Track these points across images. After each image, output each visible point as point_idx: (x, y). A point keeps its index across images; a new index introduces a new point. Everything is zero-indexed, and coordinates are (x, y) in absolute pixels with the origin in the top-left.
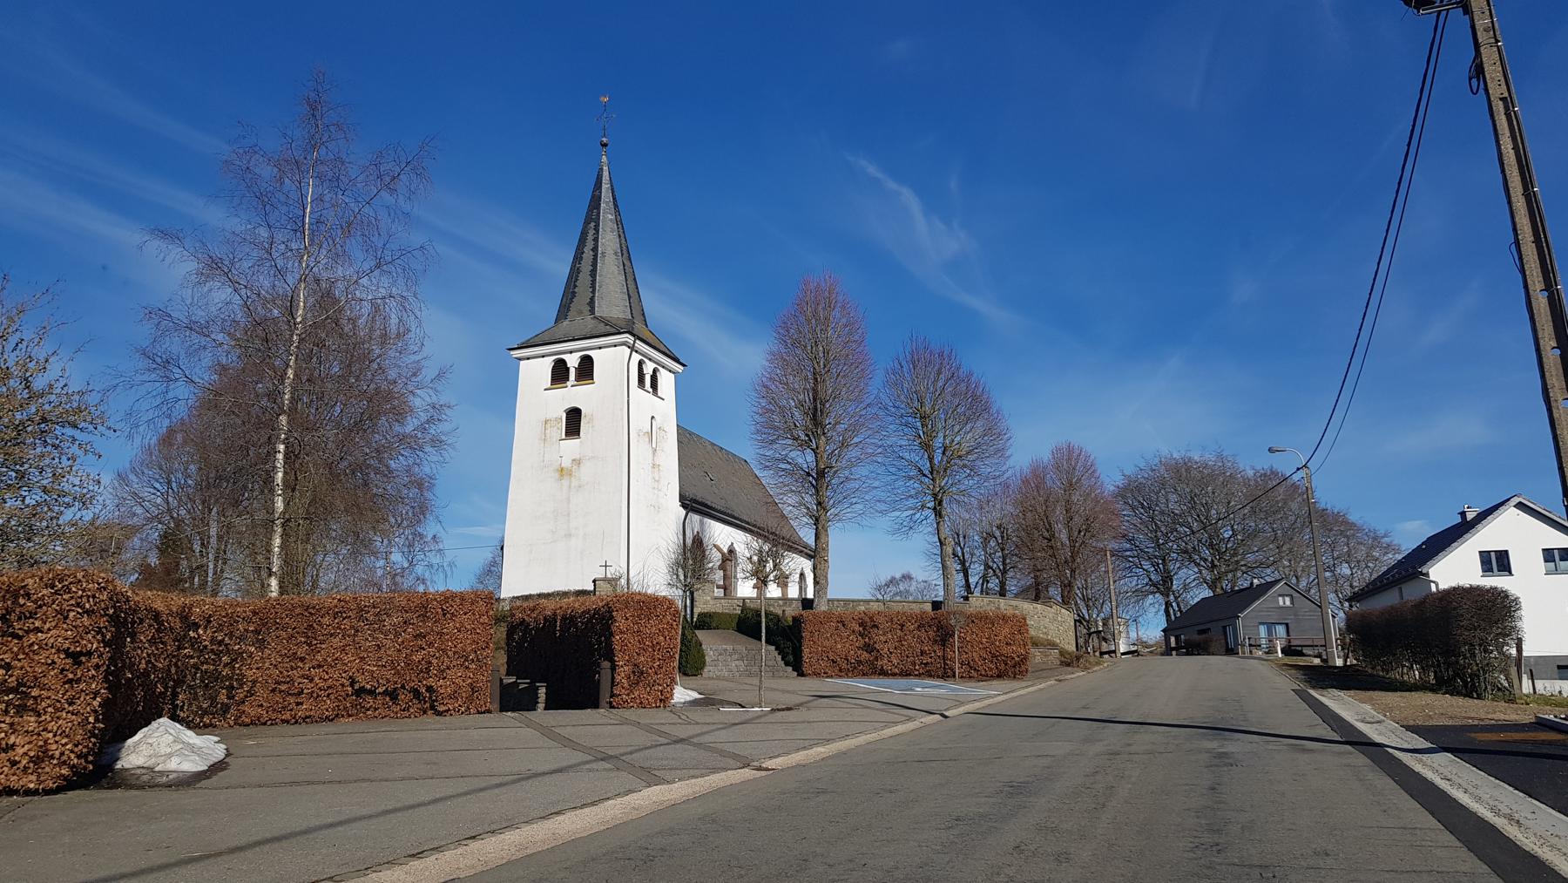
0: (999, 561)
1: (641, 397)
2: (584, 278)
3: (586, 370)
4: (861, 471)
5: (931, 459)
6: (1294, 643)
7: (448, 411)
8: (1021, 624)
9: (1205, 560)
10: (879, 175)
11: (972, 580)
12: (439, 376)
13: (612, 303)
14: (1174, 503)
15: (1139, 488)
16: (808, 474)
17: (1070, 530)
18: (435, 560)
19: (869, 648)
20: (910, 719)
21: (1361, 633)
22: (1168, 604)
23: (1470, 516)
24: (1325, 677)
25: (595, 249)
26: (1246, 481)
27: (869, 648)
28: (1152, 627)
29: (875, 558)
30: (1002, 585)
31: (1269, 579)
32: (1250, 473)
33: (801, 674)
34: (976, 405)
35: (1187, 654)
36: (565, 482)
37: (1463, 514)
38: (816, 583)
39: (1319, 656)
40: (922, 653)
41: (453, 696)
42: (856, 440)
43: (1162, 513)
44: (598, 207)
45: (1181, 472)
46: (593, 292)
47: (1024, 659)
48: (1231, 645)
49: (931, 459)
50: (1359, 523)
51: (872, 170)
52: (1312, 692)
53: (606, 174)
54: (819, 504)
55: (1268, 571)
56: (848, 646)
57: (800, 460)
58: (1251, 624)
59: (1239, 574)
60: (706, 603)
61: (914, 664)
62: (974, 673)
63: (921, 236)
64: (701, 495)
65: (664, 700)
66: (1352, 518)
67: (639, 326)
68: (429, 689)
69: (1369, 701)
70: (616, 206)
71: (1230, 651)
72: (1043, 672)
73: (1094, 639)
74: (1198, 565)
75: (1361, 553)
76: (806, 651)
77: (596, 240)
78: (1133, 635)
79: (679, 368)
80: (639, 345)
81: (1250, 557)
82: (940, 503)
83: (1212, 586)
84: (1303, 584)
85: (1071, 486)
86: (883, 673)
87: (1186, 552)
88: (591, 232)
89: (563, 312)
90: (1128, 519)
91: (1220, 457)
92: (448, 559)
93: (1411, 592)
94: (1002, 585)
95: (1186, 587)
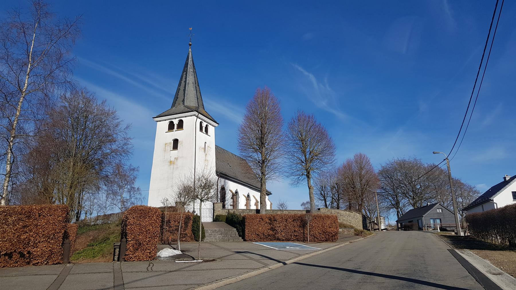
0: (337, 196)
1: (201, 136)
2: (181, 92)
3: (181, 125)
4: (278, 160)
5: (305, 156)
6: (443, 226)
7: (130, 140)
8: (335, 219)
9: (411, 196)
10: (302, 70)
11: (328, 203)
12: (127, 127)
13: (191, 100)
14: (399, 176)
15: (387, 171)
16: (259, 162)
17: (361, 184)
18: (138, 197)
19: (273, 229)
20: (266, 265)
21: (473, 222)
22: (398, 212)
23: (507, 179)
24: (459, 242)
25: (185, 82)
26: (425, 169)
27: (273, 229)
28: (392, 219)
29: (288, 194)
30: (338, 205)
31: (433, 203)
32: (426, 166)
33: (245, 240)
34: (322, 135)
35: (405, 230)
36: (172, 166)
37: (505, 178)
38: (261, 203)
39: (453, 231)
40: (295, 231)
41: (41, 256)
42: (276, 149)
43: (395, 179)
44: (187, 67)
45: (402, 165)
46: (184, 97)
47: (337, 233)
48: (421, 226)
49: (305, 156)
50: (465, 183)
51: (300, 69)
52: (456, 250)
53: (190, 55)
54: (262, 173)
55: (433, 200)
56: (264, 228)
57: (256, 157)
58: (427, 219)
59: (423, 201)
60: (219, 211)
61: (291, 236)
62: (316, 239)
63: (314, 92)
64: (224, 171)
65: (153, 257)
66: (462, 181)
67: (201, 109)
68: (29, 252)
69: (485, 257)
70: (194, 66)
71: (420, 229)
72: (345, 238)
73: (369, 225)
74: (408, 198)
75: (466, 194)
76: (247, 231)
77: (186, 78)
78: (387, 223)
79: (216, 125)
80: (200, 116)
81: (427, 195)
82: (309, 173)
83: (413, 205)
84: (445, 205)
85: (361, 168)
86: (278, 239)
87: (404, 193)
88: (185, 76)
89: (174, 105)
90: (383, 182)
91: (415, 159)
92: (143, 196)
93: (487, 208)
94: (338, 205)
95: (404, 206)
